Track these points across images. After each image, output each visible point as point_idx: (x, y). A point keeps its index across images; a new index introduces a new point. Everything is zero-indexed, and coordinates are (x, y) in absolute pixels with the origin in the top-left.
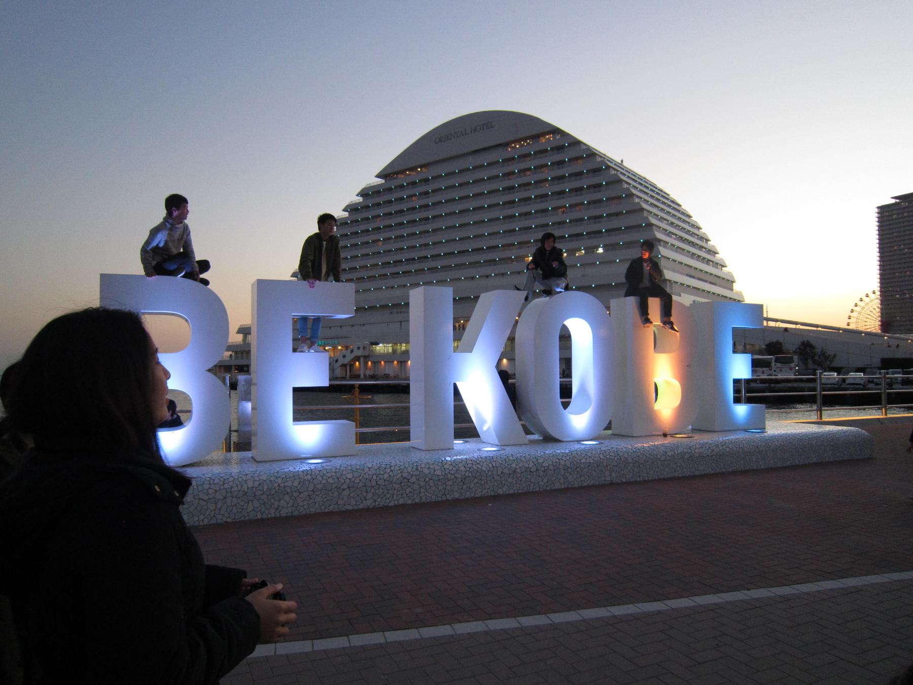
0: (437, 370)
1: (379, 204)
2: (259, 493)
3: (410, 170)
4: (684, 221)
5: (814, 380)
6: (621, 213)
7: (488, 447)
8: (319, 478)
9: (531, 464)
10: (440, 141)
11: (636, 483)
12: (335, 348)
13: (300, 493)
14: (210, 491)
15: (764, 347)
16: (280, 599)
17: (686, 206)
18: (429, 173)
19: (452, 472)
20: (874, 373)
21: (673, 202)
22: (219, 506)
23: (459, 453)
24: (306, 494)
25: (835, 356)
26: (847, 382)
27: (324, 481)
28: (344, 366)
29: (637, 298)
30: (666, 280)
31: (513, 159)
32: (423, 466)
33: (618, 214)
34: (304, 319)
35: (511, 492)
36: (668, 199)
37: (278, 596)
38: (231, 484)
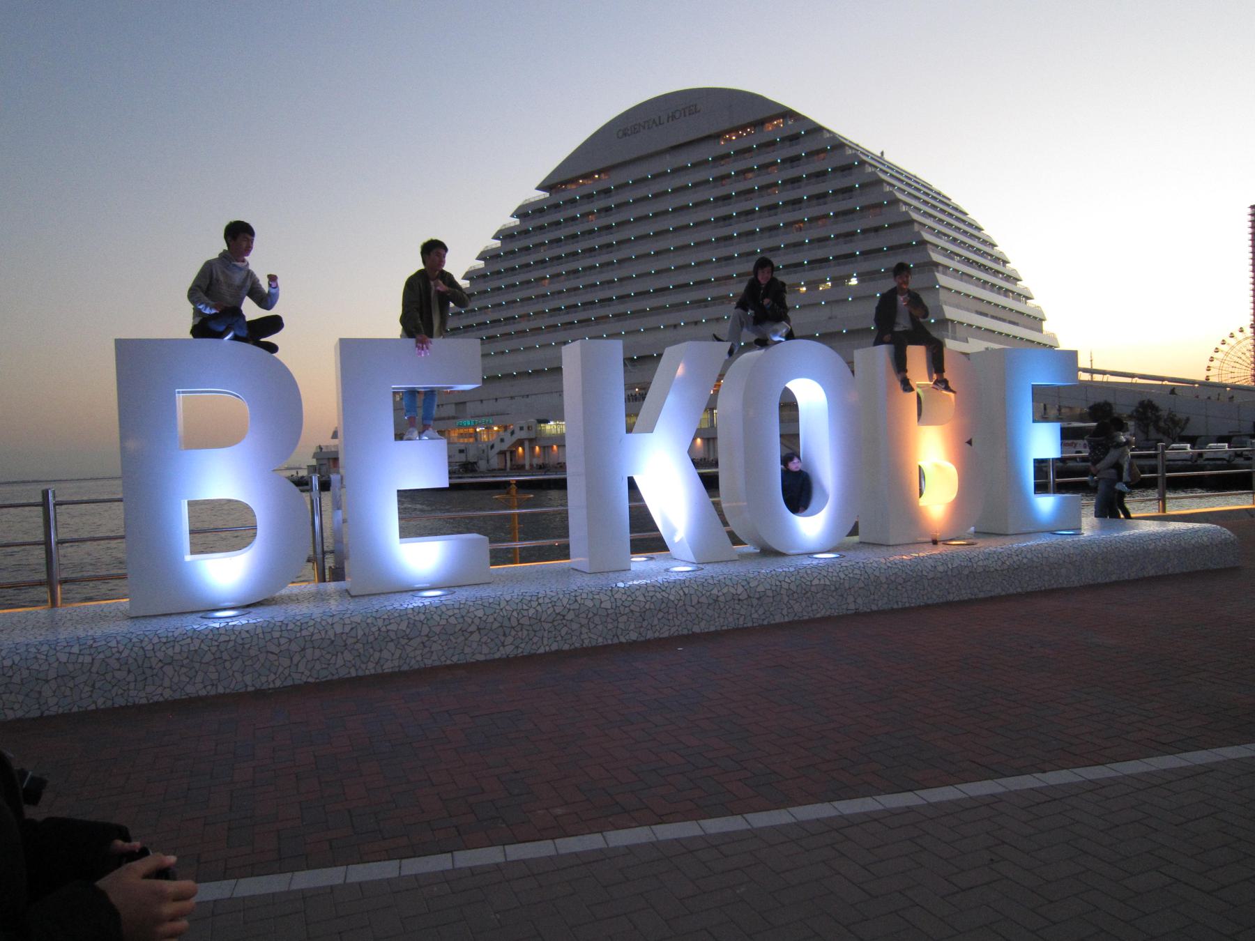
0: (601, 458)
1: (541, 228)
2: (350, 641)
3: (584, 177)
4: (972, 236)
5: (1155, 456)
6: (882, 228)
7: (681, 569)
8: (437, 618)
9: (740, 590)
10: (625, 135)
11: (893, 611)
12: (489, 428)
13: (410, 639)
14: (283, 641)
15: (1086, 410)
16: (167, 878)
17: (974, 215)
18: (610, 181)
19: (627, 604)
20: (1243, 445)
21: (956, 209)
22: (295, 662)
23: (638, 576)
24: (419, 640)
25: (1188, 419)
26: (1205, 456)
27: (443, 622)
28: (503, 453)
29: (891, 347)
30: (948, 320)
31: (728, 156)
32: (584, 596)
33: (876, 230)
34: (412, 393)
35: (712, 629)
36: (948, 205)
37: (163, 873)
38: (311, 629)
